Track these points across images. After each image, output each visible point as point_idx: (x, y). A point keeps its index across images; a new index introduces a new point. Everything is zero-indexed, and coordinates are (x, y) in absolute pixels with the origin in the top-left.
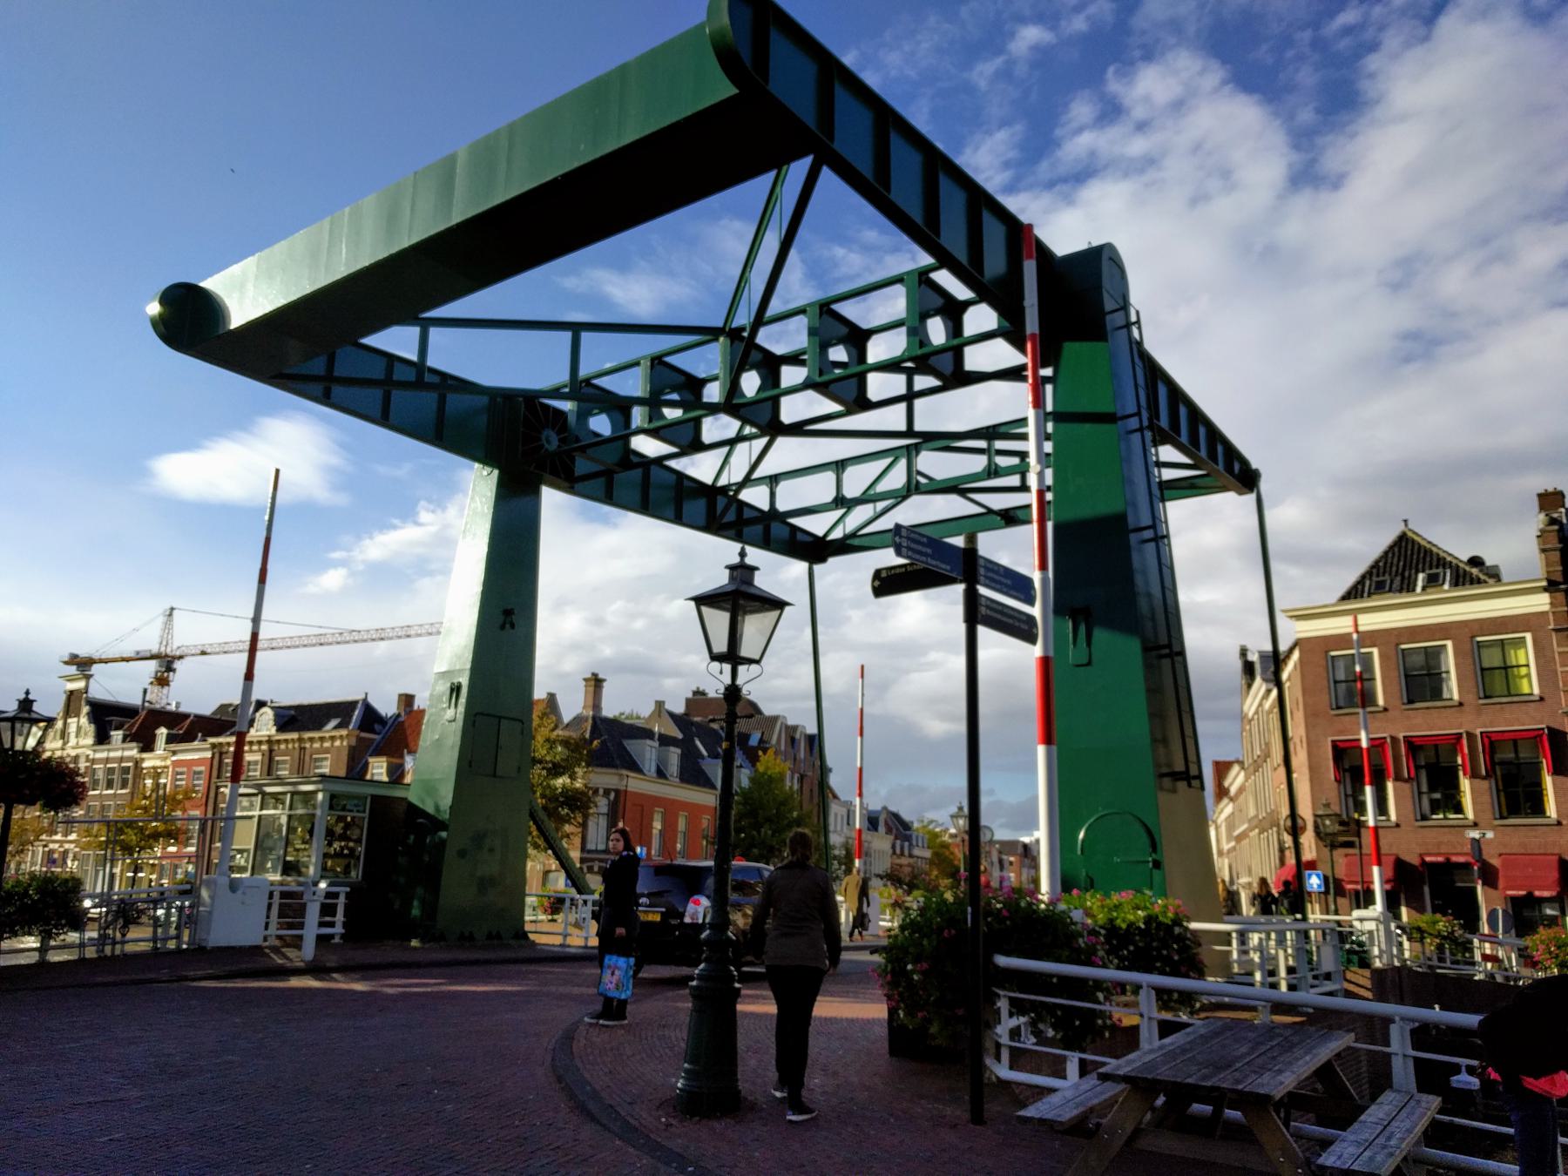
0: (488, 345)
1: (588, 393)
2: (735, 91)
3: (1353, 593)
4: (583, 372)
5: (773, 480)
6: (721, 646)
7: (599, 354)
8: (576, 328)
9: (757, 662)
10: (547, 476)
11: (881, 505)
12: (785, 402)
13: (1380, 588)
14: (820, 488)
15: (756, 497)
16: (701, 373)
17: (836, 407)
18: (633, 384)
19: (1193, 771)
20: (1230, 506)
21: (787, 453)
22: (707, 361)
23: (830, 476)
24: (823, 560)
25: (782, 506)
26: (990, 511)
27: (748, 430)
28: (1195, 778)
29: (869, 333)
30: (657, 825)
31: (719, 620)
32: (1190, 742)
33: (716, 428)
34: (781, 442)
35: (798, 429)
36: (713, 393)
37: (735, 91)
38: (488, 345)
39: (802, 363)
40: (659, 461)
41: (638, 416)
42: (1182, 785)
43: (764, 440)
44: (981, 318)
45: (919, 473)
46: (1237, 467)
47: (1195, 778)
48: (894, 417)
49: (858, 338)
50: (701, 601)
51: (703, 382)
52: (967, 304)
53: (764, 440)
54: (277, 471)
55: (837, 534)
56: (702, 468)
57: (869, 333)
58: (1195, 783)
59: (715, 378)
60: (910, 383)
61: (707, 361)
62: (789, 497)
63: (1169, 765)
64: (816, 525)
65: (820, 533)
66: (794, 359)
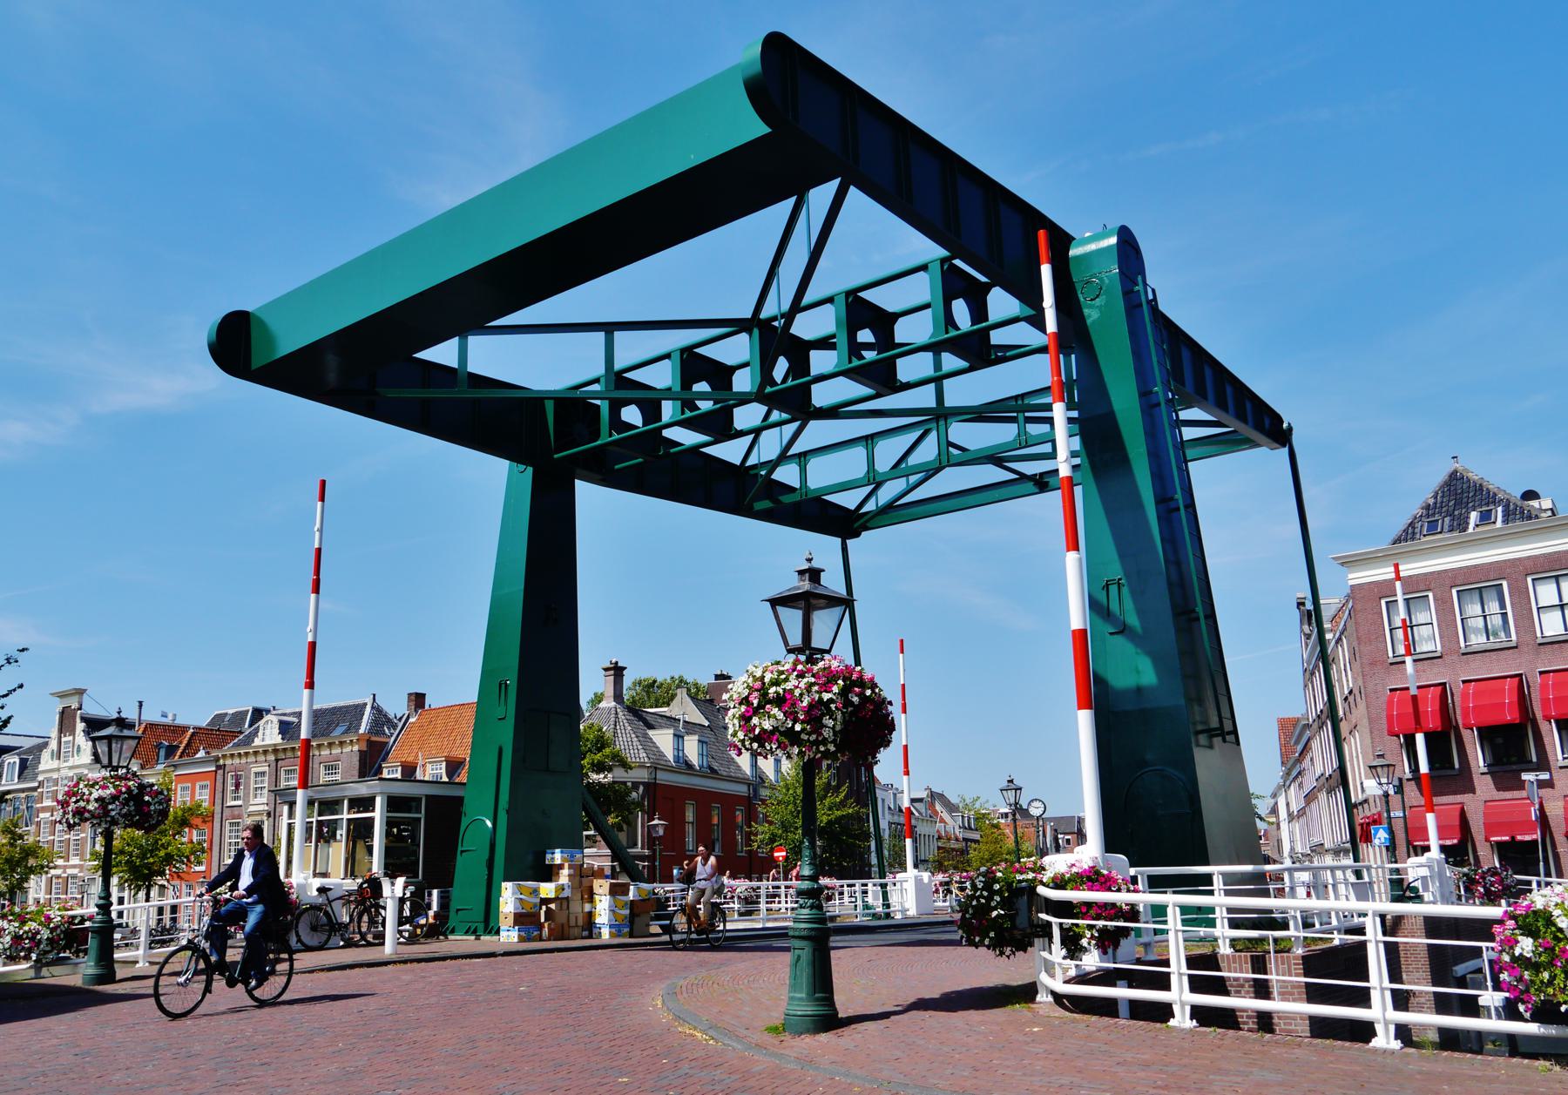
0: (525, 357)
1: (621, 384)
2: (766, 130)
3: (1409, 534)
4: (618, 366)
5: (803, 457)
6: (796, 639)
7: (630, 348)
8: (609, 328)
9: (828, 652)
10: (578, 471)
11: (914, 479)
12: (816, 389)
13: (1433, 528)
14: (852, 464)
15: (787, 474)
16: (730, 361)
17: (865, 391)
18: (662, 377)
19: (1228, 727)
20: (1267, 460)
21: (818, 433)
22: (736, 350)
23: (859, 452)
24: (857, 535)
25: (815, 483)
26: (1023, 477)
27: (776, 416)
28: (1229, 733)
29: (896, 316)
30: (690, 816)
31: (792, 618)
32: (1223, 701)
33: (747, 416)
34: (813, 424)
35: (832, 413)
36: (743, 382)
37: (766, 130)
38: (525, 357)
39: (833, 347)
40: (695, 450)
41: (668, 410)
42: (1217, 741)
43: (795, 425)
44: (1001, 303)
45: (950, 444)
46: (1267, 422)
47: (1229, 733)
48: (924, 398)
49: (884, 322)
50: (775, 602)
51: (732, 370)
52: (986, 288)
53: (795, 425)
54: (323, 483)
55: (870, 506)
56: (730, 452)
57: (896, 316)
58: (1230, 738)
59: (746, 365)
60: (938, 365)
61: (736, 350)
62: (821, 474)
63: (1206, 722)
64: (849, 500)
65: (852, 507)
66: (825, 343)
